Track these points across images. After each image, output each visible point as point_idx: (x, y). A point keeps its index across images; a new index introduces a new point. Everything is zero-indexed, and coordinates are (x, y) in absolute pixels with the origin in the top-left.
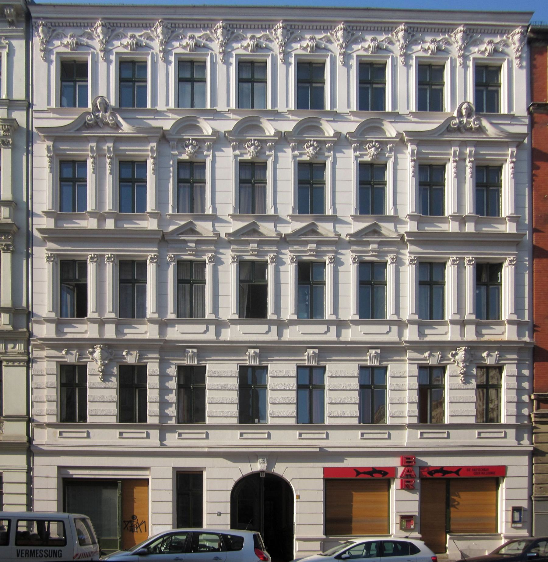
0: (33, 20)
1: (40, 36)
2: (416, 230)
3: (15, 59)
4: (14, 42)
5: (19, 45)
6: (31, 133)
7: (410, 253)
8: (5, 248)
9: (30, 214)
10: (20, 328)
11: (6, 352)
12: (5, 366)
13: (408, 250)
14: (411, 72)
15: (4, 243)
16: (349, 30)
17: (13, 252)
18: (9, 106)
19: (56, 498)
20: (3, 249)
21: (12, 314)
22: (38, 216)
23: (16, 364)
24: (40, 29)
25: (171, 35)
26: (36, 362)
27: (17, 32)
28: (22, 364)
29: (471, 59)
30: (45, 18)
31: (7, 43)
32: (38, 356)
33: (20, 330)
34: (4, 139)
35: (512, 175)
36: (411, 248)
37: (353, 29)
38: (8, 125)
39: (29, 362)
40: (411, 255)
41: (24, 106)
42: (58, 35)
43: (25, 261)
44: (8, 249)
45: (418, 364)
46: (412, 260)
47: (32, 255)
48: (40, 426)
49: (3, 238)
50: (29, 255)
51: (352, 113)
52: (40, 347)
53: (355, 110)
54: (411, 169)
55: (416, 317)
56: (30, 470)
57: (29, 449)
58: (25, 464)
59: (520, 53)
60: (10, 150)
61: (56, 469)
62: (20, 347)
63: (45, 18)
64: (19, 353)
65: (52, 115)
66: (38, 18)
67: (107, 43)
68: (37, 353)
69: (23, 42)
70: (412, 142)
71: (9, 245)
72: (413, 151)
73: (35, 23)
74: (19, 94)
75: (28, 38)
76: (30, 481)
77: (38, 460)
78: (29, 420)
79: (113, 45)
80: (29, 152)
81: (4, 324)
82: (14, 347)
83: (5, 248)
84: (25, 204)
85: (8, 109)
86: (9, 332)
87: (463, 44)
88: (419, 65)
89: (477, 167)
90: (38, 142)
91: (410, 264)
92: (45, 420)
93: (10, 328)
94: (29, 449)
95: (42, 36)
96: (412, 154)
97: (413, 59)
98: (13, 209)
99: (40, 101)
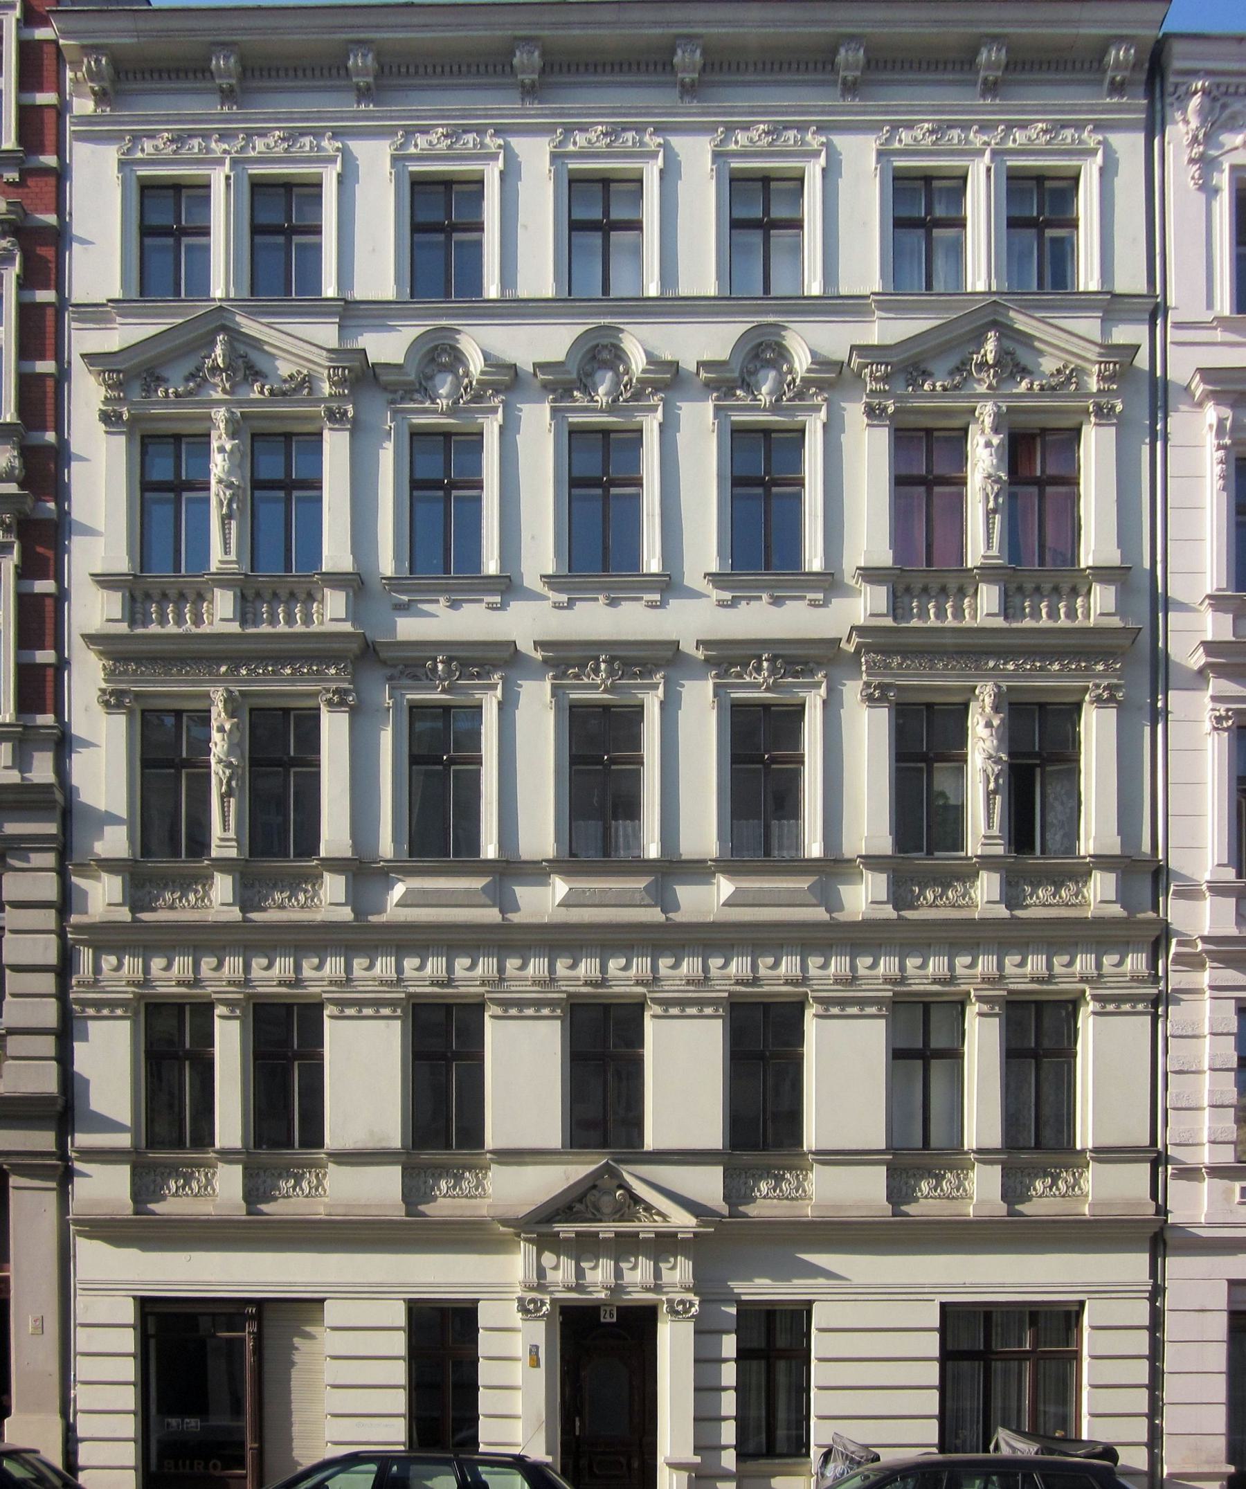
0: (1172, 79)
1: (1187, 122)
2: (1230, 637)
3: (1118, 182)
4: (1117, 140)
5: (1129, 145)
6: (1160, 385)
7: (1214, 699)
8: (113, 701)
9: (1160, 603)
10: (372, 914)
11: (349, 980)
12: (222, 1017)
13: (1210, 692)
14: (1216, 205)
15: (334, 686)
16: (1215, 93)
17: (354, 712)
18: (1106, 311)
19: (1223, 1368)
20: (330, 703)
21: (350, 877)
22: (1184, 607)
23: (1126, 1007)
24: (1195, 101)
25: (1221, 114)
26: (1178, 1002)
27: (1129, 111)
28: (1140, 1007)
29: (1226, 166)
30: (1209, 73)
31: (338, 149)
32: (1182, 986)
33: (1140, 916)
34: (334, 405)
35: (1221, 482)
36: (1216, 685)
37: (1226, 93)
38: (344, 368)
39: (1158, 1004)
40: (1218, 706)
41: (1140, 311)
42: (1233, 117)
43: (1147, 730)
44: (342, 703)
45: (1237, 999)
46: (1219, 719)
47: (1167, 712)
48: (1190, 1173)
49: (333, 671)
50: (1158, 715)
51: (1221, 322)
52: (1192, 962)
53: (1227, 313)
54: (1218, 469)
55: (1230, 874)
56: (1157, 1292)
57: (1159, 1238)
58: (1144, 1275)
59: (1201, 148)
60: (347, 434)
61: (1224, 1286)
62: (1136, 962)
63: (1209, 73)
64: (383, 983)
65: (1219, 335)
66: (1194, 73)
67: (1209, 138)
68: (1177, 979)
69: (1140, 138)
70: (1217, 397)
71: (1117, 687)
72: (1221, 422)
73: (1177, 86)
74: (1131, 279)
75: (1153, 127)
76: (1156, 1323)
77: (1175, 1266)
78: (1158, 1160)
79: (1221, 146)
80: (1158, 436)
81: (331, 904)
82: (421, 968)
83: (113, 701)
84: (1148, 574)
85: (1103, 320)
86: (1113, 922)
87: (1202, 126)
88: (1238, 190)
89: (1237, 459)
90: (1183, 407)
91: (1215, 729)
92: (1205, 1156)
93: (1117, 910)
94: (1159, 1238)
95: (1194, 123)
96: (1220, 430)
97: (1223, 171)
98: (354, 594)
99: (1182, 297)
